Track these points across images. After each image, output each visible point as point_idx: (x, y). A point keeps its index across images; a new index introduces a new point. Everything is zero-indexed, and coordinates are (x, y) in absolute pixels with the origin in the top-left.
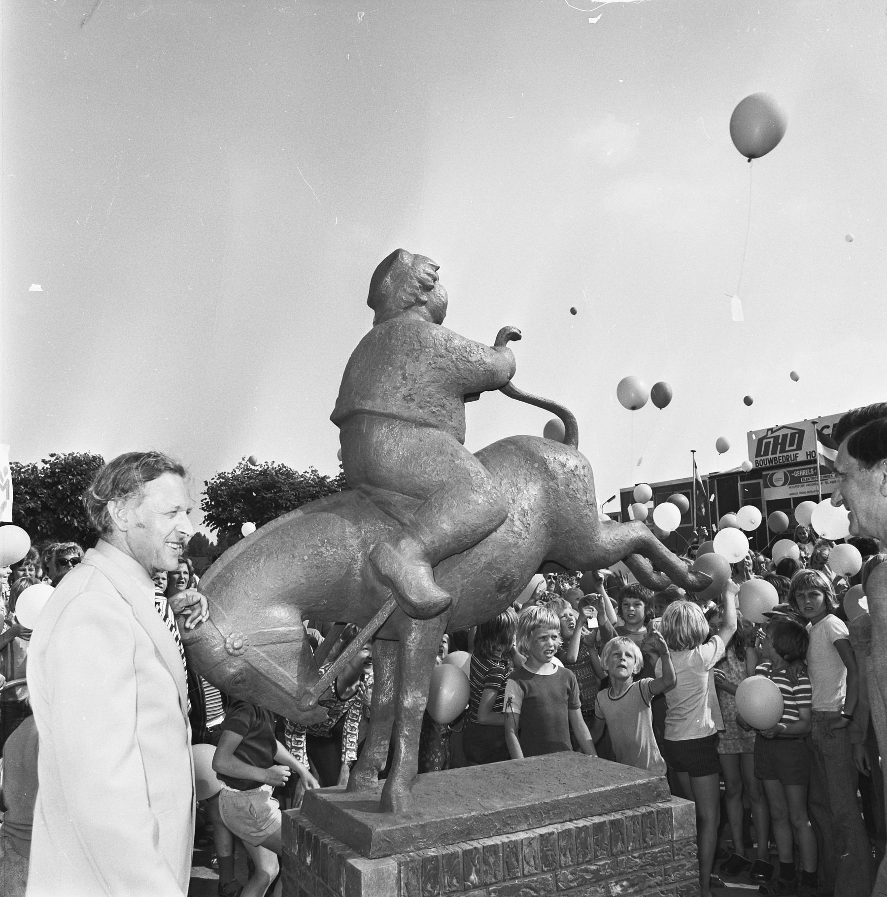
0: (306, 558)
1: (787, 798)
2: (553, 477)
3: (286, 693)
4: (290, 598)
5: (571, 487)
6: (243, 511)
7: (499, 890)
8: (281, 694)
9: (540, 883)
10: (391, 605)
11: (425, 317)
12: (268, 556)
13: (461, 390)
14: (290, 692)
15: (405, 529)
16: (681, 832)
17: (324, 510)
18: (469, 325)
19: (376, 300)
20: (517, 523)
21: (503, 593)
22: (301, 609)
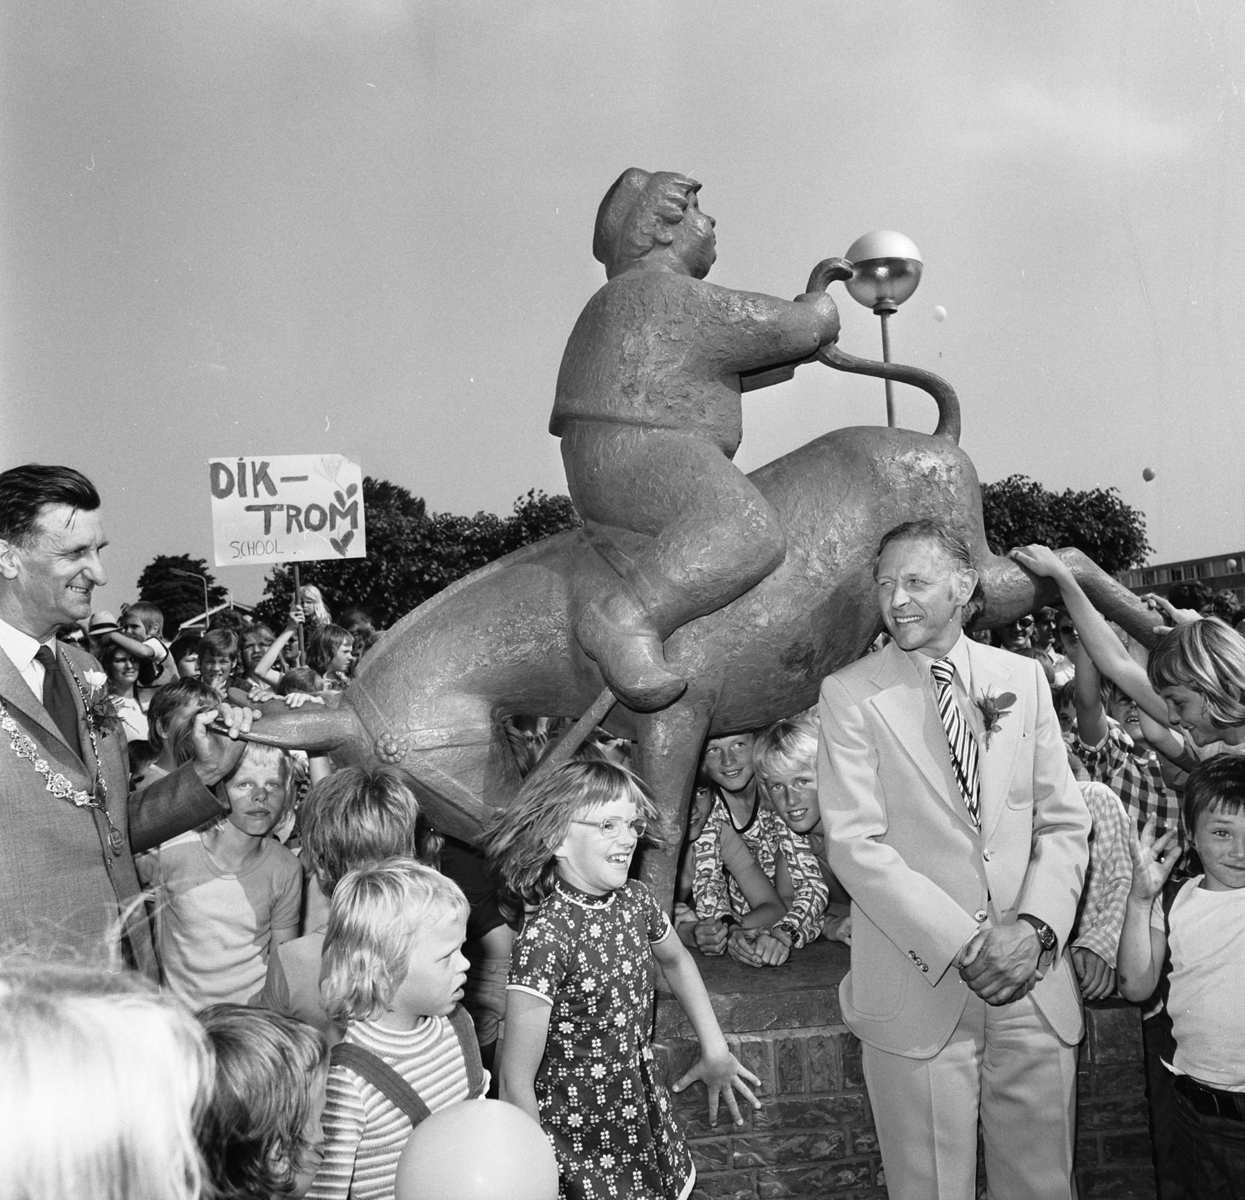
0: (490, 629)
1: (450, 1048)
2: (887, 490)
3: (466, 814)
4: (470, 687)
5: (921, 502)
6: (376, 569)
7: (769, 1108)
8: (462, 816)
9: (842, 1105)
10: (608, 697)
11: (671, 266)
12: (440, 629)
13: (717, 368)
14: (472, 813)
15: (627, 581)
16: (1112, 1051)
17: (530, 560)
18: (760, 267)
19: (604, 247)
20: (818, 566)
21: (798, 670)
22: (489, 700)
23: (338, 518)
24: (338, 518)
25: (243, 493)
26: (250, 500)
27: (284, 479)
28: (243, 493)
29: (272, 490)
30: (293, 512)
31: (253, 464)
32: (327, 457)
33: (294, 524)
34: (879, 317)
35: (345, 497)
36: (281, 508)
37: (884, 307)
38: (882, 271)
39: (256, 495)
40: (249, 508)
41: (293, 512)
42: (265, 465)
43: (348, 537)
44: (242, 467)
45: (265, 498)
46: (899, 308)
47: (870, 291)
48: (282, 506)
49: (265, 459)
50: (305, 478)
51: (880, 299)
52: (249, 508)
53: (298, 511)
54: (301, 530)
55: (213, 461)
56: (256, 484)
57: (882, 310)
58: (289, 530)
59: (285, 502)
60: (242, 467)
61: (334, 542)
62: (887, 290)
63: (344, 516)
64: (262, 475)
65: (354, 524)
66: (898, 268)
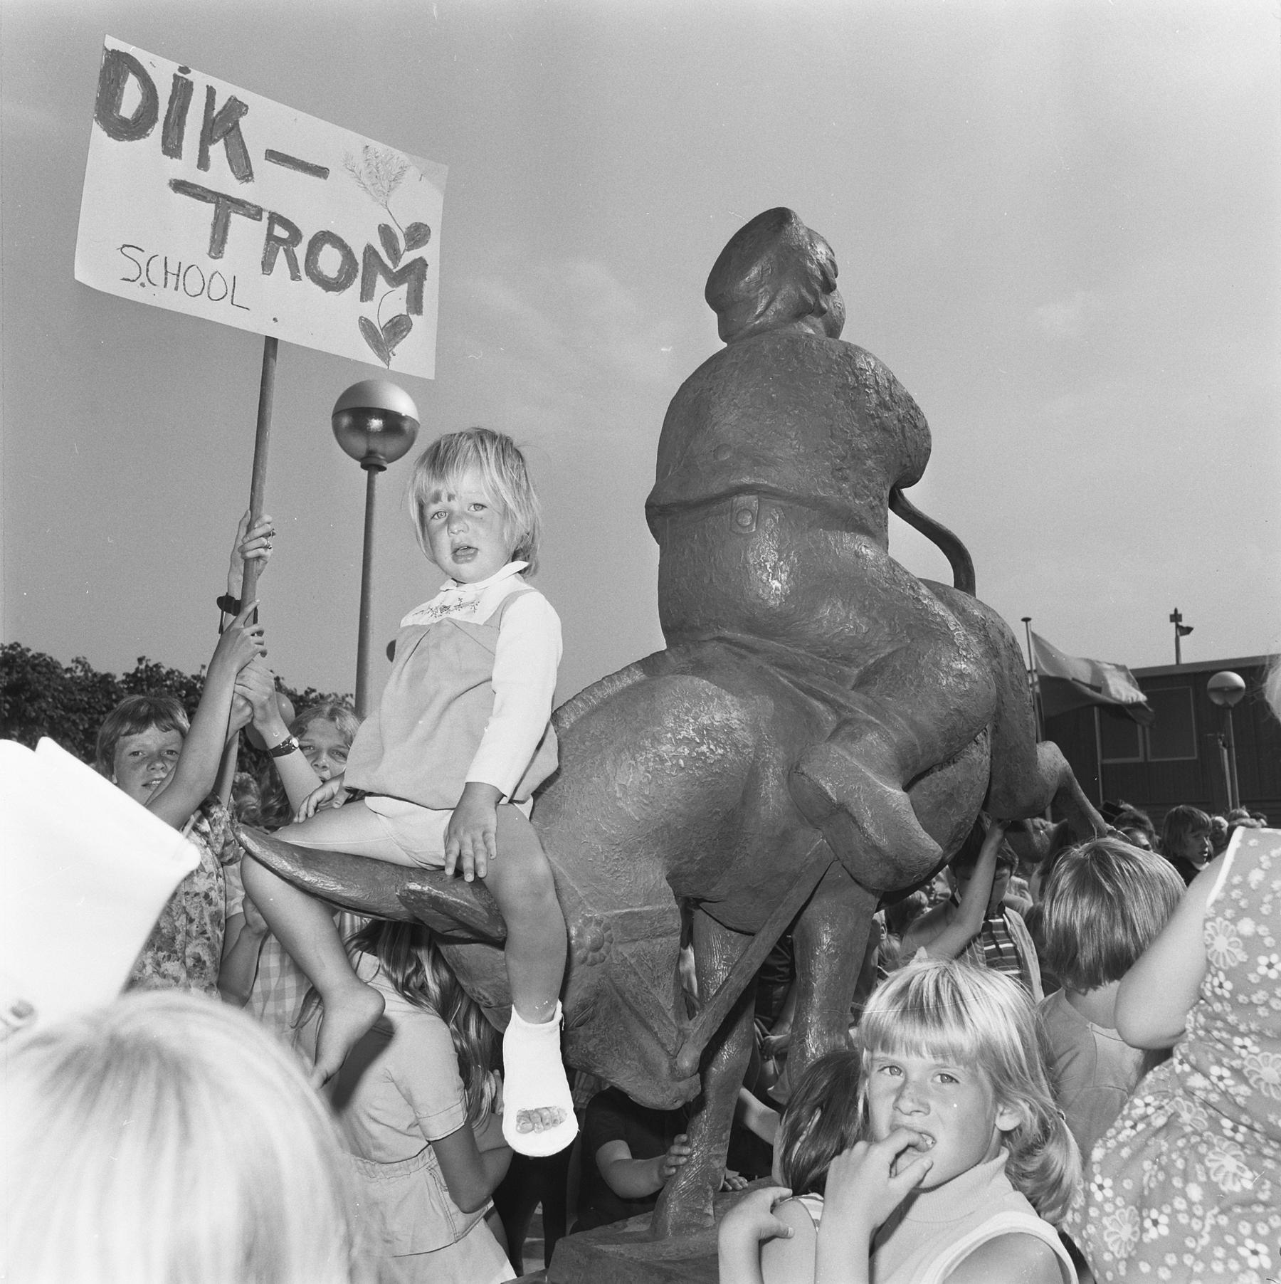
23: (381, 281)
24: (381, 281)
25: (172, 148)
26: (184, 167)
27: (272, 155)
28: (172, 148)
29: (245, 173)
30: (280, 232)
31: (211, 92)
32: (378, 147)
33: (281, 257)
34: (365, 473)
35: (402, 244)
36: (256, 213)
37: (374, 461)
38: (376, 424)
39: (203, 163)
40: (180, 186)
41: (280, 232)
42: (236, 108)
43: (398, 327)
44: (182, 90)
45: (220, 177)
46: (388, 466)
47: (360, 444)
48: (259, 211)
49: (243, 95)
50: (321, 172)
51: (371, 453)
52: (180, 186)
53: (296, 235)
54: (295, 277)
55: (113, 43)
56: (207, 139)
57: (372, 464)
58: (267, 266)
59: (269, 205)
60: (182, 90)
61: (367, 326)
62: (377, 445)
63: (395, 279)
64: (224, 124)
65: (415, 303)
66: (394, 422)
